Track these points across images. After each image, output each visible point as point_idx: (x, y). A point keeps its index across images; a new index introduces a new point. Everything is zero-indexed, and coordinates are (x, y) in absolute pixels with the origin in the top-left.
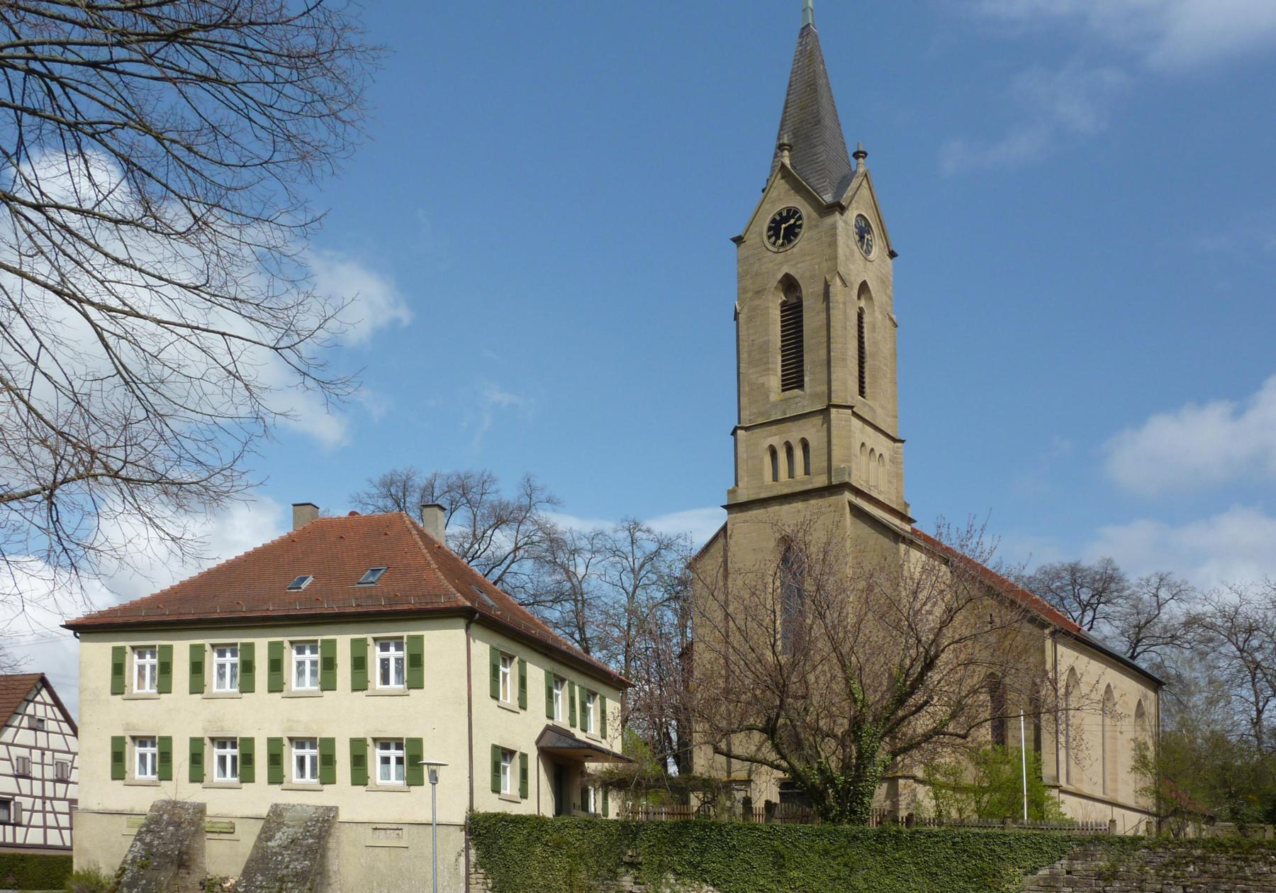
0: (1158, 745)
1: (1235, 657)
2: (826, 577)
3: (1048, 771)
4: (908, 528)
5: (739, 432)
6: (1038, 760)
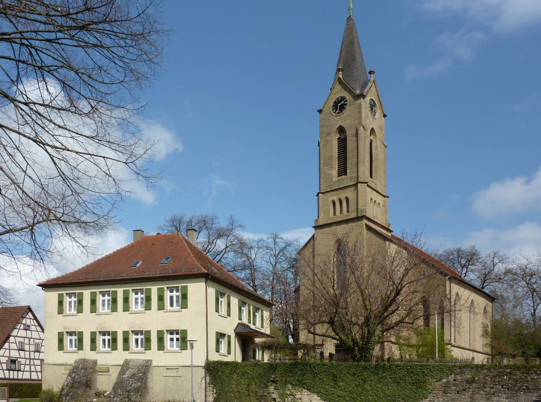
0: (492, 325)
1: (525, 287)
3: (446, 337)
4: (390, 234)
5: (320, 195)
6: (442, 333)
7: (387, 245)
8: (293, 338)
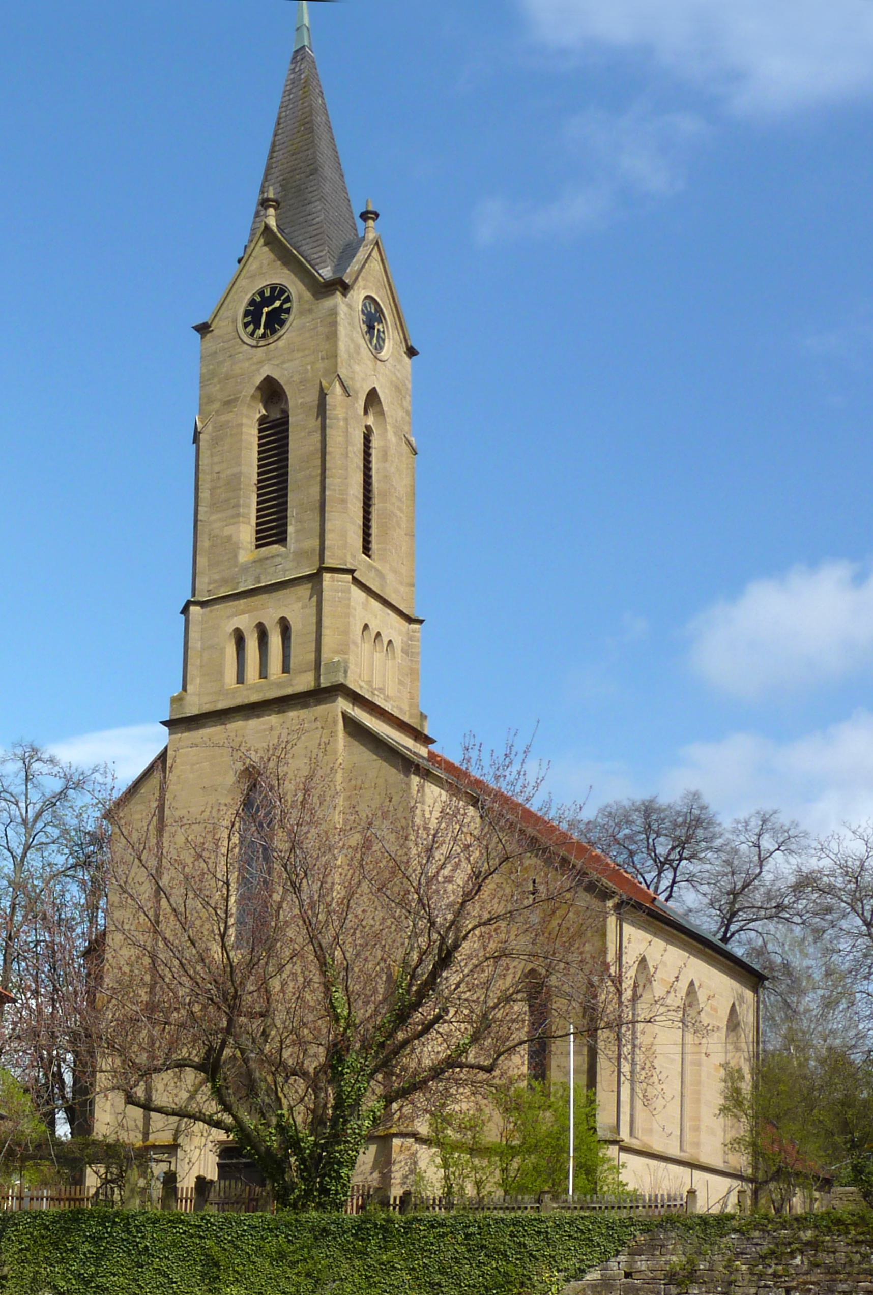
0: (756, 1071)
1: (861, 935)
2: (305, 829)
3: (604, 1119)
4: (423, 751)
5: (193, 609)
6: (591, 1102)
7: (414, 789)
8: (71, 1121)
